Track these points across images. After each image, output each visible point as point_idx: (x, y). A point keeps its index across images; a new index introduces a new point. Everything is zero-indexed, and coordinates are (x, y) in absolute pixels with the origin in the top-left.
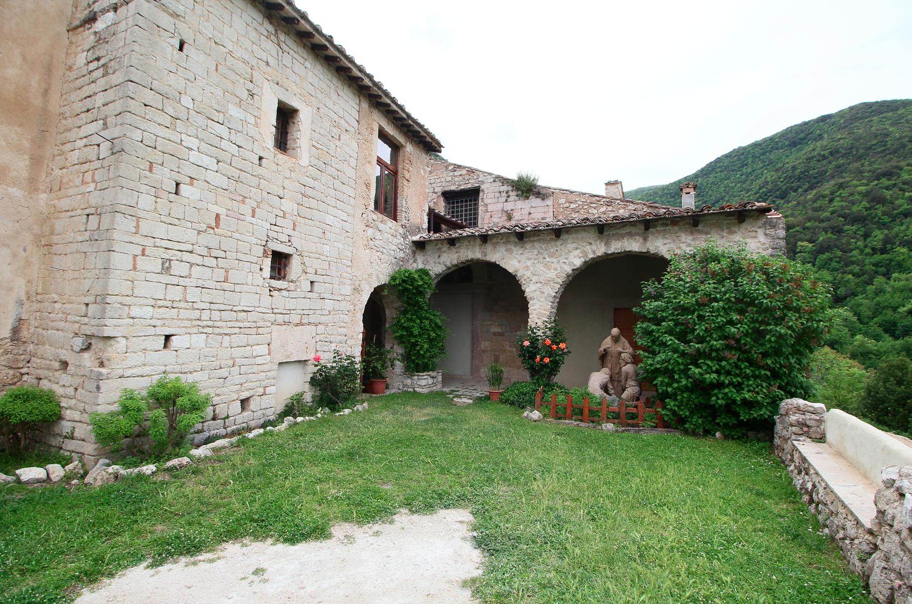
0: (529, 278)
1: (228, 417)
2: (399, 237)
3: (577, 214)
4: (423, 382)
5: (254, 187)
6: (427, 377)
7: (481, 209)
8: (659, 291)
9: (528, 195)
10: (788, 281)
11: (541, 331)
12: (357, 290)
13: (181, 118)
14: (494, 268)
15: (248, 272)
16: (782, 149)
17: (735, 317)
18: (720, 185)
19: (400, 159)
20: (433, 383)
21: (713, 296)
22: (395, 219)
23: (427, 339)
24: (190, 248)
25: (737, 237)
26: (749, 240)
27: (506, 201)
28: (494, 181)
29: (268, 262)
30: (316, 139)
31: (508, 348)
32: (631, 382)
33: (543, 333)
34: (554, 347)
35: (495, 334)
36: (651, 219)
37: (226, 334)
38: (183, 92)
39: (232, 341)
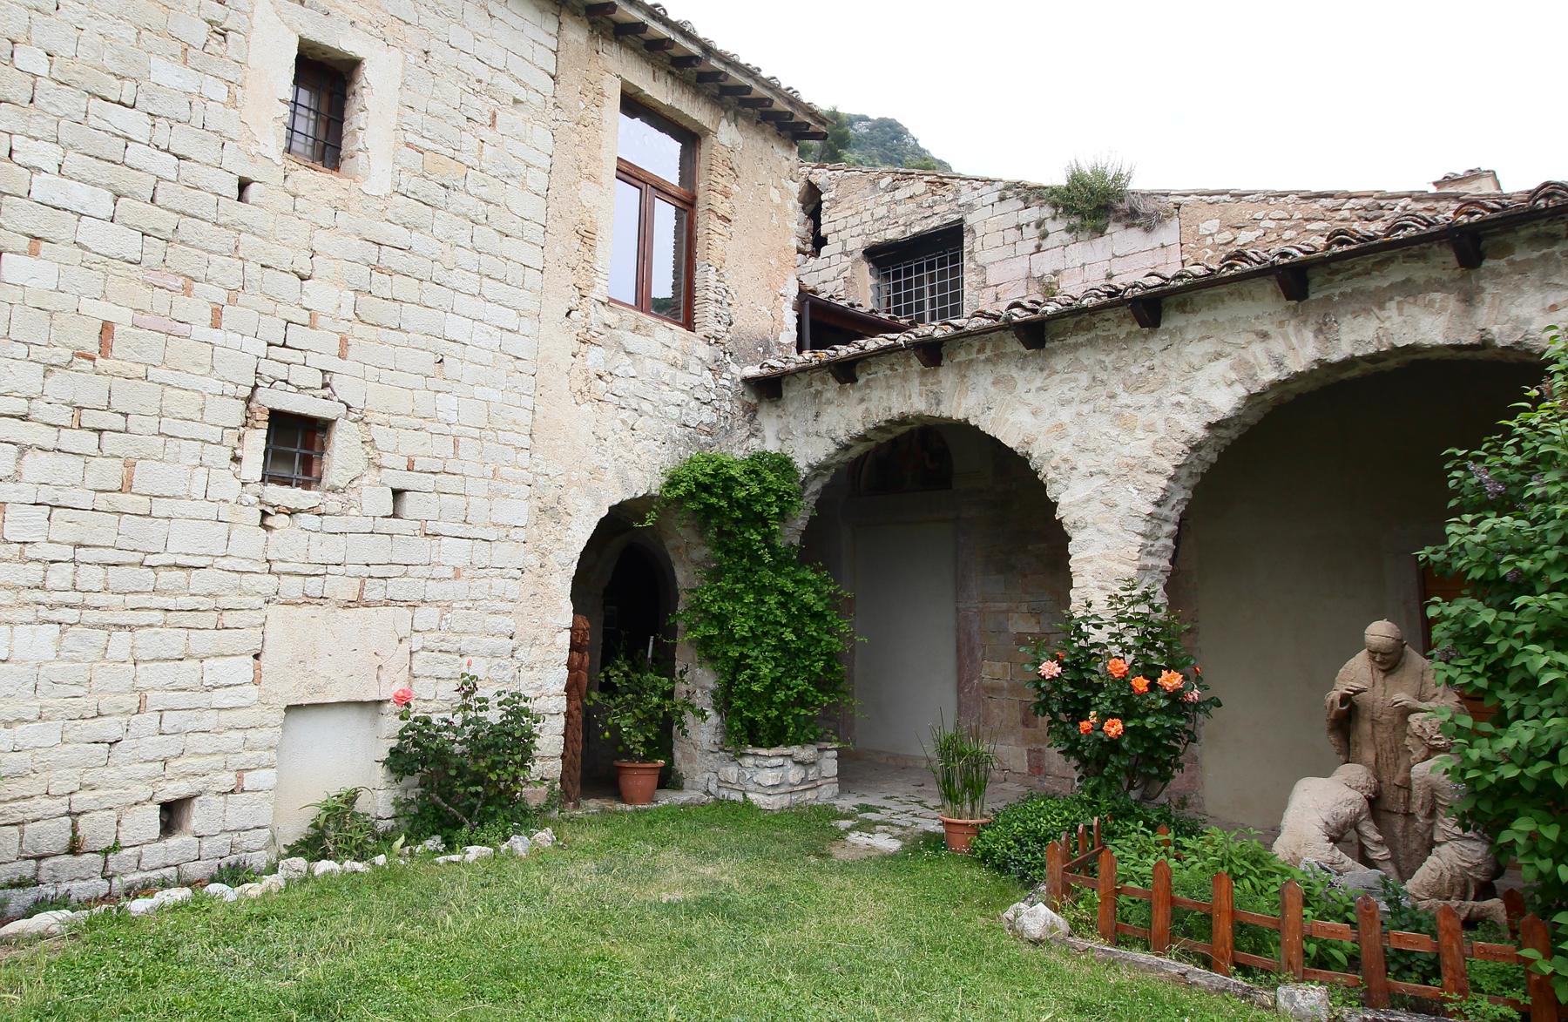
0: (1066, 461)
1: (116, 848)
2: (695, 367)
4: (769, 777)
5: (221, 254)
6: (780, 761)
7: (969, 278)
9: (1100, 223)
11: (1107, 629)
12: (550, 512)
13: (12, 98)
15: (195, 467)
19: (702, 165)
20: (803, 781)
22: (689, 324)
23: (775, 648)
24: (20, 406)
27: (1038, 249)
28: (1002, 199)
29: (257, 440)
30: (415, 127)
32: (1447, 825)
35: (1021, 639)
36: (1478, 223)
37: (120, 627)
38: (22, 39)
39: (139, 643)
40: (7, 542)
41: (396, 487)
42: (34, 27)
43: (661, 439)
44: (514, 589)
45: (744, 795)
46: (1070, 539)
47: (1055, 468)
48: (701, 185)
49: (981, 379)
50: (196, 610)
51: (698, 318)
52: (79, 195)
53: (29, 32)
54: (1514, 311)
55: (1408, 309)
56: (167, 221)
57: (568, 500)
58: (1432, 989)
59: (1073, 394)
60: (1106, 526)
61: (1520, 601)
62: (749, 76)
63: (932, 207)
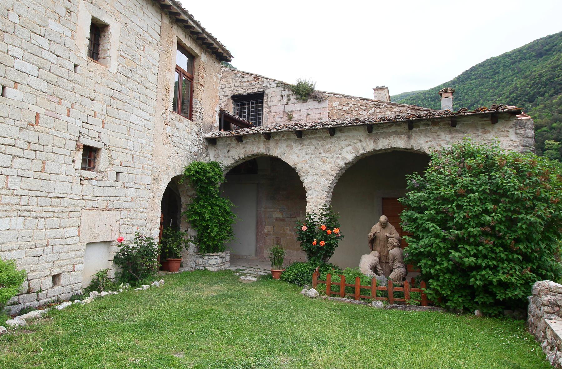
0: (306, 170)
1: (41, 291)
2: (194, 134)
3: (349, 115)
5: (69, 91)
7: (265, 110)
8: (422, 183)
9: (306, 98)
10: (537, 175)
11: (318, 217)
12: (156, 180)
13: (8, 31)
14: (276, 162)
15: (63, 164)
16: (529, 59)
17: (490, 206)
18: (475, 90)
19: (196, 67)
20: (222, 263)
21: (469, 188)
22: (191, 118)
23: (217, 223)
24: (12, 142)
25: (491, 136)
26: (501, 139)
27: (287, 103)
28: (277, 86)
29: (80, 155)
30: (123, 50)
31: (288, 232)
32: (398, 264)
33: (319, 219)
34: (329, 232)
35: (277, 219)
36: (415, 120)
37: (41, 218)
38: (11, 9)
39: (47, 223)
40: (9, 189)
41: (117, 171)
42: (14, 6)
43: (184, 156)
44: (147, 204)
45: (205, 268)
46: (307, 192)
47: (303, 172)
48: (195, 74)
49: (283, 145)
50: (62, 212)
51: (193, 117)
52: (29, 68)
53: (13, 7)
54: (419, 142)
55: (396, 138)
56: (54, 78)
57: (161, 176)
58: (402, 299)
59: (310, 152)
60: (317, 189)
62: (213, 40)
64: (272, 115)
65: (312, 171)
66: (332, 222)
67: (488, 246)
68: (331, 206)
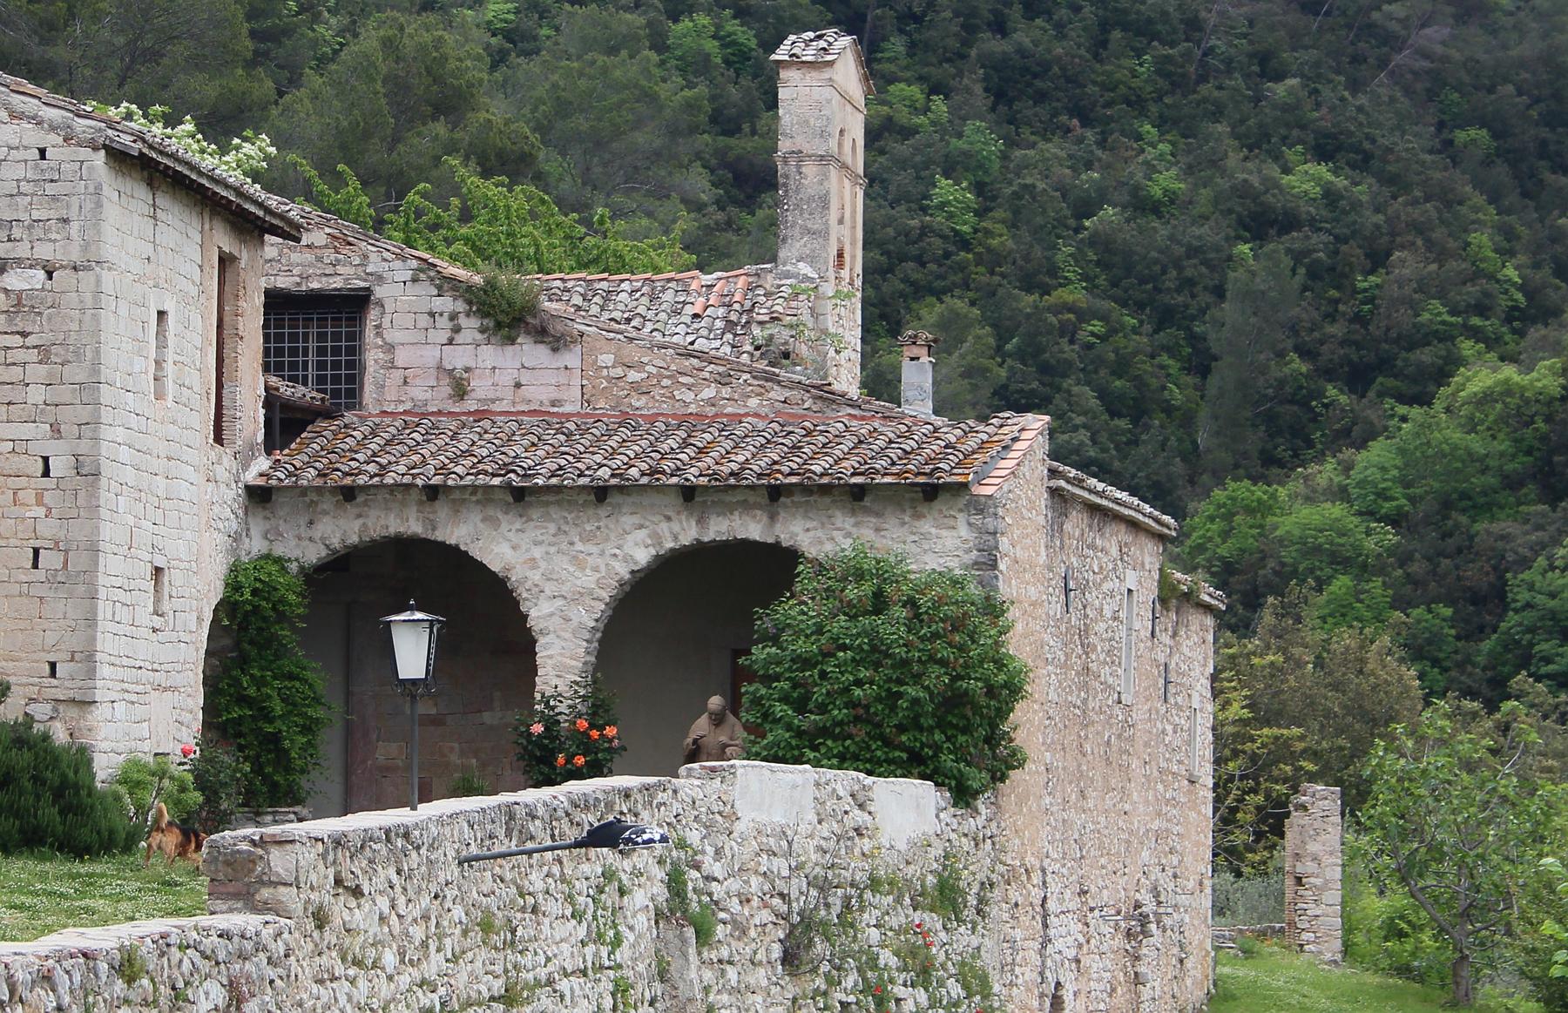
0: (536, 585)
3: (644, 399)
7: (373, 358)
9: (513, 333)
12: (200, 619)
14: (458, 562)
17: (864, 673)
21: (841, 641)
25: (926, 526)
26: (944, 533)
27: (450, 342)
28: (415, 280)
31: (455, 758)
33: (570, 707)
34: (595, 734)
46: (536, 642)
54: (792, 528)
60: (563, 634)
61: (774, 685)
63: (334, 266)
64: (397, 375)
65: (550, 588)
66: (599, 711)
67: (857, 739)
68: (599, 675)
